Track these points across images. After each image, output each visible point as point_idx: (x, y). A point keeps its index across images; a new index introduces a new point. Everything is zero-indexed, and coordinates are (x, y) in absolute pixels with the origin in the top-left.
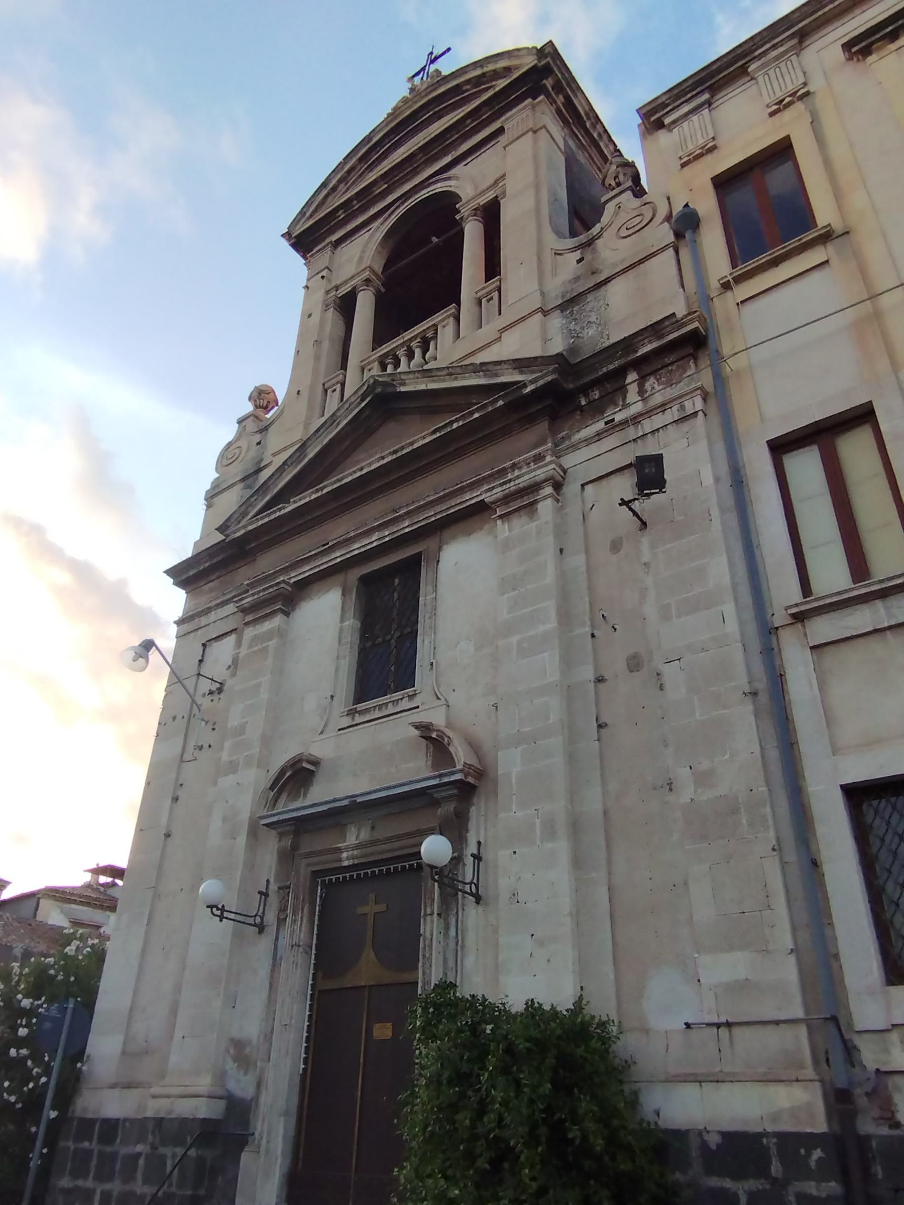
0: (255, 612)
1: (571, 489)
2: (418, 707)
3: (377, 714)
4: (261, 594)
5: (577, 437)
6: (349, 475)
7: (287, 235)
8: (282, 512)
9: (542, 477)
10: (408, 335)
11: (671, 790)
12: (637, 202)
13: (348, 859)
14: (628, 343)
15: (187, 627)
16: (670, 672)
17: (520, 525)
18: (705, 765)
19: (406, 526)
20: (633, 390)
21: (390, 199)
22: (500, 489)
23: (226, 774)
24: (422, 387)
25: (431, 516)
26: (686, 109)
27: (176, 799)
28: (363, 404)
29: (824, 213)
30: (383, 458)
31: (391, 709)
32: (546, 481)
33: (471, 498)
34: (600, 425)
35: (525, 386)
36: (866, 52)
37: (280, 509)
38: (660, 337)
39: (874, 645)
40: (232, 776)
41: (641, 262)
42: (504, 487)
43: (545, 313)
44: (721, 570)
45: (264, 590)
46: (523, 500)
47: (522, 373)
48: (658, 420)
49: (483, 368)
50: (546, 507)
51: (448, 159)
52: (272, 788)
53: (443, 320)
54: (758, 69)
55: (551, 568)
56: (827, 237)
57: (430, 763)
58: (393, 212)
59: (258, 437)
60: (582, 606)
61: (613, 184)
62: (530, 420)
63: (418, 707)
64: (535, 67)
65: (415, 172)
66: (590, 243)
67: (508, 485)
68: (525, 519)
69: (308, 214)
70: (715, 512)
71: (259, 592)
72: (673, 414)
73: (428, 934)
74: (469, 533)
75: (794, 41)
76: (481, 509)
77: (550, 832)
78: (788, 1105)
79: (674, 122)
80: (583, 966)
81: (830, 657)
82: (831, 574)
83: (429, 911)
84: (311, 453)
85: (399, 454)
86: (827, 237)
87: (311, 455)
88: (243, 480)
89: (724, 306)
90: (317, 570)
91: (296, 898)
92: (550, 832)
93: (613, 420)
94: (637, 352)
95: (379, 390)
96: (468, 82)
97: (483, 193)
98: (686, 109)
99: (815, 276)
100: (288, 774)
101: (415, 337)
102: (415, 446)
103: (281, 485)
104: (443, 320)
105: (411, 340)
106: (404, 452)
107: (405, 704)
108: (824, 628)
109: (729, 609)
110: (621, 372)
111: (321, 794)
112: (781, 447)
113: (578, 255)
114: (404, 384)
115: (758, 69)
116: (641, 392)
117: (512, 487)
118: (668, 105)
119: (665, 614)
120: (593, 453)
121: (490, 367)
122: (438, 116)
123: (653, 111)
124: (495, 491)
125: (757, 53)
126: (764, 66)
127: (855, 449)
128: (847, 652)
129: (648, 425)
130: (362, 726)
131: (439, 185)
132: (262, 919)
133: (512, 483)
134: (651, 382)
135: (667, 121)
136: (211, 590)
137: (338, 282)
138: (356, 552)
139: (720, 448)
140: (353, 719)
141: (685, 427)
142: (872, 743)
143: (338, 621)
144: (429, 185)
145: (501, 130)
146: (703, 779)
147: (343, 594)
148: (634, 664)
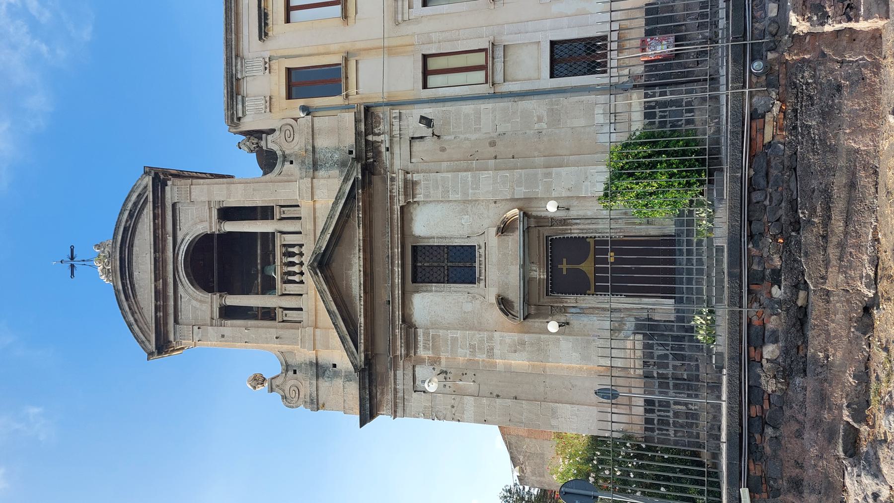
0: (410, 343)
1: (410, 167)
3: (483, 266)
5: (388, 164)
7: (150, 354)
12: (277, 133)
14: (358, 134)
15: (400, 411)
16: (500, 130)
18: (536, 119)
19: (397, 251)
20: (376, 138)
21: (170, 280)
24: (328, 236)
26: (240, 106)
27: (498, 396)
29: (336, 59)
31: (483, 259)
36: (266, 34)
39: (508, 64)
41: (313, 131)
43: (313, 178)
44: (467, 108)
46: (410, 187)
48: (396, 128)
50: (416, 177)
51: (170, 240)
52: (507, 315)
54: (242, 74)
55: (445, 175)
56: (346, 59)
60: (464, 164)
62: (370, 183)
65: (164, 262)
68: (418, 187)
69: (144, 339)
70: (444, 109)
75: (239, 59)
77: (548, 175)
78: (637, 100)
79: (243, 112)
80: (597, 163)
81: (509, 78)
82: (480, 76)
84: (334, 308)
86: (346, 59)
87: (335, 308)
88: (317, 378)
89: (354, 99)
91: (557, 302)
92: (548, 175)
95: (316, 264)
96: (127, 221)
97: (210, 217)
98: (240, 106)
99: (360, 65)
103: (344, 329)
105: (282, 278)
108: (499, 77)
109: (483, 106)
110: (366, 141)
111: (515, 296)
112: (425, 86)
115: (242, 74)
116: (379, 134)
117: (402, 190)
119: (478, 130)
120: (397, 160)
123: (232, 119)
126: (242, 71)
127: (433, 64)
128: (508, 73)
129: (396, 132)
134: (376, 131)
135: (240, 115)
136: (382, 393)
137: (209, 316)
139: (416, 106)
141: (404, 117)
142: (539, 69)
143: (430, 294)
144: (178, 254)
145: (174, 205)
146: (540, 120)
147: (417, 292)
148: (493, 144)
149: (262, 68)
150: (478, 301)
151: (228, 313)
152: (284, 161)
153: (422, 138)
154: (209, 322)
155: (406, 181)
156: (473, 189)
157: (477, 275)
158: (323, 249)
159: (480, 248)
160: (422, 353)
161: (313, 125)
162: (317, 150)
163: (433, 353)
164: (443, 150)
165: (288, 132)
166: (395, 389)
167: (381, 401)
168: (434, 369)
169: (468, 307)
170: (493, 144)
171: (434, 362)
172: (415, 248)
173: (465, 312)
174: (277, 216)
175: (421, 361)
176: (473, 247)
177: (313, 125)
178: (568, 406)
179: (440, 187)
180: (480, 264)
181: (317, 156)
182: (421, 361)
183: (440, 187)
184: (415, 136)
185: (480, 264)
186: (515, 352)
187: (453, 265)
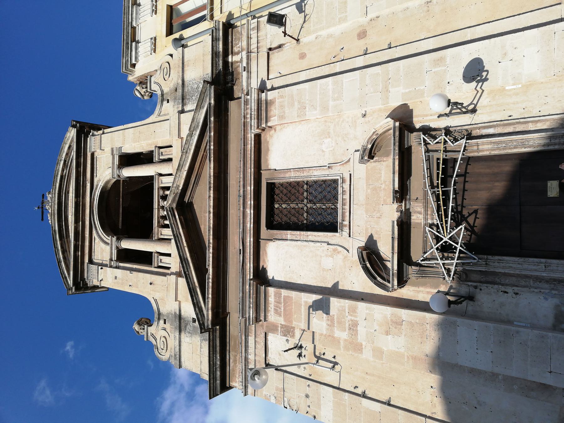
2: (350, 175)
3: (347, 207)
4: (251, 301)
6: (208, 236)
8: (211, 277)
9: (256, 95)
10: (156, 206)
11: (430, 2)
13: (432, 219)
17: (274, 111)
21: (87, 223)
22: (253, 121)
23: (356, 334)
24: (185, 173)
25: (250, 171)
28: (177, 217)
30: (210, 197)
31: (347, 197)
32: (258, 95)
33: (251, 137)
34: (245, 74)
35: (210, 104)
37: (209, 278)
38: (219, 40)
40: (359, 328)
41: (183, 63)
42: (253, 118)
45: (250, 297)
46: (262, 110)
47: (203, 107)
48: (254, 41)
49: (190, 135)
51: (88, 185)
53: (158, 182)
57: (385, 159)
58: (94, 223)
59: (162, 322)
61: (144, 90)
63: (350, 175)
64: (77, 130)
66: (159, 314)
67: (253, 116)
71: (250, 302)
72: (254, 34)
73: (490, 146)
74: (268, 150)
75: (134, 44)
76: (258, 137)
79: (136, 58)
83: (475, 148)
85: (212, 185)
88: (180, 331)
90: (252, 257)
93: (245, 67)
94: (219, 52)
96: (63, 170)
100: (368, 265)
101: (159, 202)
102: (212, 174)
104: (158, 182)
105: (159, 222)
106: (212, 182)
107: (346, 186)
111: (387, 249)
113: (165, 102)
114: (179, 186)
117: (254, 113)
118: (128, 60)
121: (193, 125)
122: (67, 192)
124: (253, 124)
125: (130, 21)
129: (254, 47)
130: (351, 219)
131: (97, 193)
132: (476, 105)
133: (253, 113)
135: (134, 62)
138: (252, 226)
140: (345, 226)
144: (94, 199)
145: (93, 154)
149: (150, 11)
150: (340, 256)
151: (393, 222)
152: (162, 100)
153: (280, 46)
154: (108, 263)
155: (259, 101)
156: (334, 100)
157: (339, 220)
158: (181, 188)
159: (343, 181)
160: (272, 317)
161: (183, 57)
162: (186, 83)
163: (285, 321)
164: (302, 56)
165: (165, 70)
166: (246, 359)
167: (234, 370)
168: (287, 340)
169: (328, 263)
170: (362, 35)
171: (288, 331)
172: (271, 187)
173: (324, 270)
174: (156, 159)
175: (274, 328)
176: (335, 181)
177: (183, 57)
178: (532, 129)
179: (296, 103)
180: (343, 204)
181: (186, 90)
182: (274, 328)
183: (296, 103)
184: (273, 46)
185: (343, 204)
186: (387, 333)
187: (308, 207)
